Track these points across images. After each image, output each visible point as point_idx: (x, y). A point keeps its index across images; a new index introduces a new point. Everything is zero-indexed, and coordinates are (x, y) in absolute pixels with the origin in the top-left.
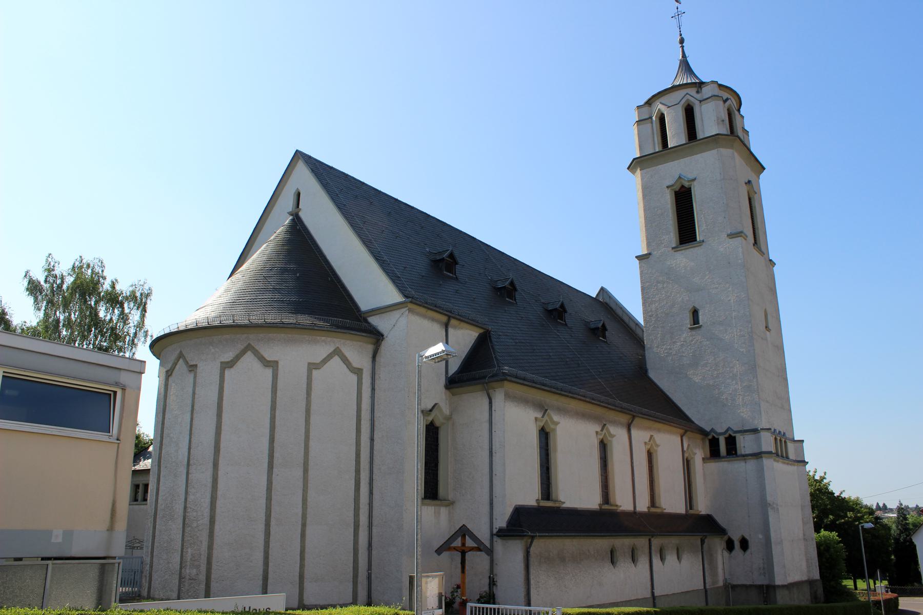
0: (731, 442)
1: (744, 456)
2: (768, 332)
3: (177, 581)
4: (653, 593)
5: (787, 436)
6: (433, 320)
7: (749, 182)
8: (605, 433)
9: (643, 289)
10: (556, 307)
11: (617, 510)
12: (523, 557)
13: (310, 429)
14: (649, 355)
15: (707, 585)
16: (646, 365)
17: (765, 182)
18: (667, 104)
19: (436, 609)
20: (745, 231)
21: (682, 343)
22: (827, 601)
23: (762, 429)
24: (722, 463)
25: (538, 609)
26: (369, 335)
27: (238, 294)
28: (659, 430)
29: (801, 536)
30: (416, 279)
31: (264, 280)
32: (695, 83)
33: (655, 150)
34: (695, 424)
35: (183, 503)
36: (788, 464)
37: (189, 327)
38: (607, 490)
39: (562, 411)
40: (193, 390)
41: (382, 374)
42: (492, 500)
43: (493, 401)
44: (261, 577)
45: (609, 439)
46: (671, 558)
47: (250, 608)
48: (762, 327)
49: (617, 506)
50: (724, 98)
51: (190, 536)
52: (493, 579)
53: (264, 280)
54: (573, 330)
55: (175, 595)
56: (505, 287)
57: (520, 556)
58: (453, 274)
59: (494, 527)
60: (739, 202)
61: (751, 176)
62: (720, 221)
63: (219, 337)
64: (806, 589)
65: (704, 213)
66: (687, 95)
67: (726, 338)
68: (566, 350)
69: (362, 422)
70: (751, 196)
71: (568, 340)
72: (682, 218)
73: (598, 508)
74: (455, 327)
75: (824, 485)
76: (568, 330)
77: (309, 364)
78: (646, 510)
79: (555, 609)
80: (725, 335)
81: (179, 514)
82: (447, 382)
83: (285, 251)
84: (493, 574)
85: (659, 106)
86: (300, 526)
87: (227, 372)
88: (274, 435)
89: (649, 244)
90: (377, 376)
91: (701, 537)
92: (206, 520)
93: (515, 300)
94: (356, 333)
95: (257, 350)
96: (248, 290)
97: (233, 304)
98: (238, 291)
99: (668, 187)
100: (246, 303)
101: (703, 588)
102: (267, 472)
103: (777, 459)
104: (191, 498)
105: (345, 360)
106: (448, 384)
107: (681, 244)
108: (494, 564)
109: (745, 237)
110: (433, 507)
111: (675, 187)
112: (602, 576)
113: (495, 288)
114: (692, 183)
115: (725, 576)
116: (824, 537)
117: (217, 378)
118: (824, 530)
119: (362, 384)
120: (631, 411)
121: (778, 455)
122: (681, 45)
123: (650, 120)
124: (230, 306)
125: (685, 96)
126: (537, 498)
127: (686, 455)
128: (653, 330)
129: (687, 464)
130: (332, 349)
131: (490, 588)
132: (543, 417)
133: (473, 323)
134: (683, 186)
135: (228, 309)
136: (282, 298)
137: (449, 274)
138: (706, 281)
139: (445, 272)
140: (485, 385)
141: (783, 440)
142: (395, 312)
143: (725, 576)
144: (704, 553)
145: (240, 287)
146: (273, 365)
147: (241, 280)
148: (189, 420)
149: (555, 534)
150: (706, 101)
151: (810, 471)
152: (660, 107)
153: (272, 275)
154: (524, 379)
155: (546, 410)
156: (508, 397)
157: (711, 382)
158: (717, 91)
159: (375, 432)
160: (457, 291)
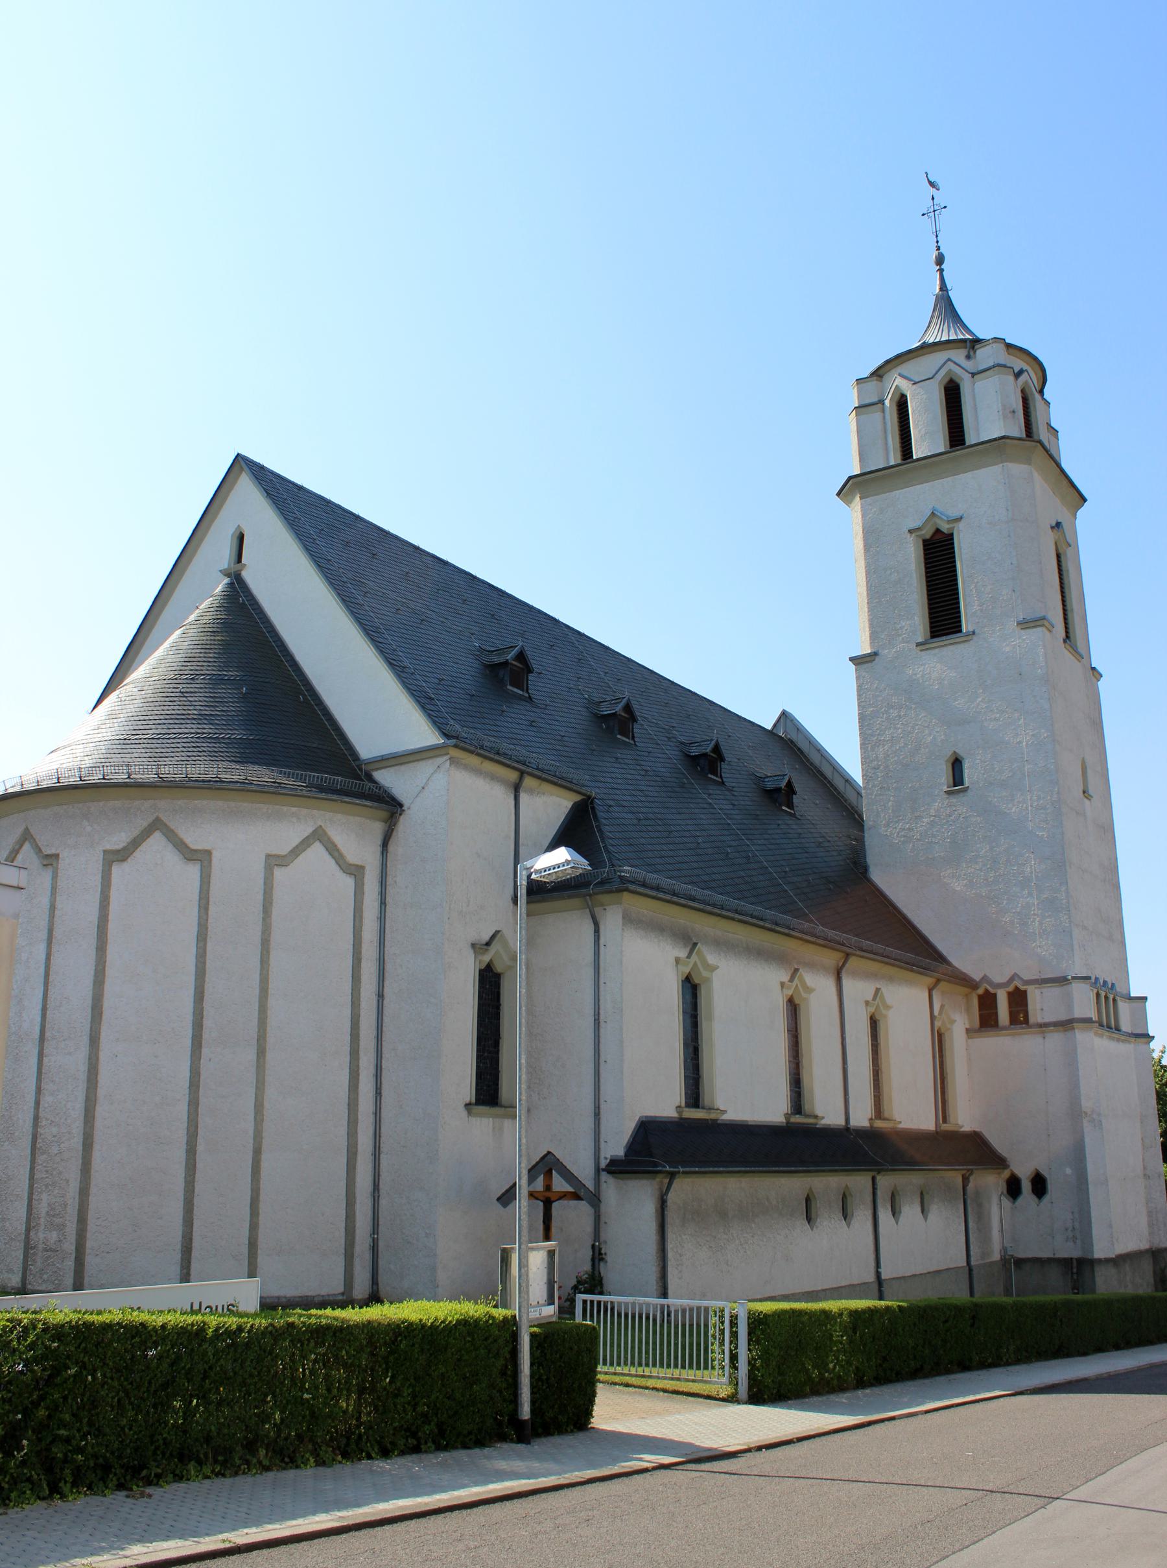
0: (1018, 999)
1: (1041, 1026)
2: (1087, 801)
3: (20, 1254)
4: (878, 1275)
5: (1118, 990)
6: (493, 777)
7: (1058, 525)
8: (797, 985)
9: (862, 718)
11: (816, 1124)
12: (654, 1210)
13: (270, 976)
14: (872, 842)
15: (972, 1259)
16: (865, 857)
17: (1085, 522)
18: (912, 378)
19: (544, 1305)
20: (1049, 616)
23: (1074, 978)
25: (686, 1302)
26: (376, 804)
27: (134, 723)
28: (891, 979)
30: (462, 701)
31: (181, 699)
32: (964, 341)
33: (888, 459)
34: (955, 967)
35: (32, 1110)
36: (1118, 1040)
37: (44, 784)
38: (800, 1088)
39: (723, 945)
40: (51, 902)
41: (399, 876)
42: (599, 1107)
43: (602, 928)
44: (179, 1247)
45: (804, 995)
46: (910, 1211)
47: (200, 1303)
49: (816, 1117)
50: (1016, 371)
51: (47, 1171)
52: (600, 1249)
53: (181, 699)
54: (735, 793)
55: (69, 1280)
57: (649, 1208)
58: (523, 691)
59: (602, 1156)
61: (1063, 516)
63: (101, 804)
64: (1147, 1266)
65: (976, 580)
67: (1013, 810)
68: (726, 832)
69: (364, 964)
70: (1061, 551)
71: (728, 812)
72: (934, 585)
74: (531, 791)
76: (727, 793)
77: (269, 856)
78: (865, 1124)
79: (735, 1305)
80: (1010, 806)
81: (24, 1130)
83: (219, 644)
84: (599, 1241)
85: (897, 382)
86: (252, 1153)
87: (116, 870)
88: (203, 986)
89: (874, 636)
90: (390, 880)
91: (964, 1172)
92: (77, 1142)
93: (633, 738)
94: (358, 801)
95: (172, 831)
96: (151, 718)
97: (125, 742)
98: (132, 719)
99: (910, 531)
100: (150, 741)
101: (965, 1264)
102: (189, 1053)
103: (1100, 1031)
104: (46, 1100)
105: (333, 850)
107: (933, 637)
111: (923, 532)
112: (791, 1244)
113: (595, 715)
114: (955, 525)
115: (1003, 1243)
117: (97, 880)
120: (843, 944)
122: (938, 267)
123: (880, 405)
124: (119, 747)
125: (945, 363)
126: (678, 1104)
127: (937, 1024)
128: (880, 795)
129: (939, 1040)
130: (310, 830)
131: (593, 1265)
132: (689, 957)
134: (938, 531)
135: (116, 751)
136: (216, 733)
137: (516, 690)
139: (509, 687)
141: (1111, 997)
143: (1003, 1243)
144: (969, 1202)
145: (138, 710)
146: (201, 858)
147: (138, 697)
148: (44, 957)
149: (711, 1169)
152: (900, 382)
153: (196, 690)
154: (657, 888)
155: (695, 944)
156: (629, 920)
158: (1003, 357)
159: (387, 983)
160: (531, 723)
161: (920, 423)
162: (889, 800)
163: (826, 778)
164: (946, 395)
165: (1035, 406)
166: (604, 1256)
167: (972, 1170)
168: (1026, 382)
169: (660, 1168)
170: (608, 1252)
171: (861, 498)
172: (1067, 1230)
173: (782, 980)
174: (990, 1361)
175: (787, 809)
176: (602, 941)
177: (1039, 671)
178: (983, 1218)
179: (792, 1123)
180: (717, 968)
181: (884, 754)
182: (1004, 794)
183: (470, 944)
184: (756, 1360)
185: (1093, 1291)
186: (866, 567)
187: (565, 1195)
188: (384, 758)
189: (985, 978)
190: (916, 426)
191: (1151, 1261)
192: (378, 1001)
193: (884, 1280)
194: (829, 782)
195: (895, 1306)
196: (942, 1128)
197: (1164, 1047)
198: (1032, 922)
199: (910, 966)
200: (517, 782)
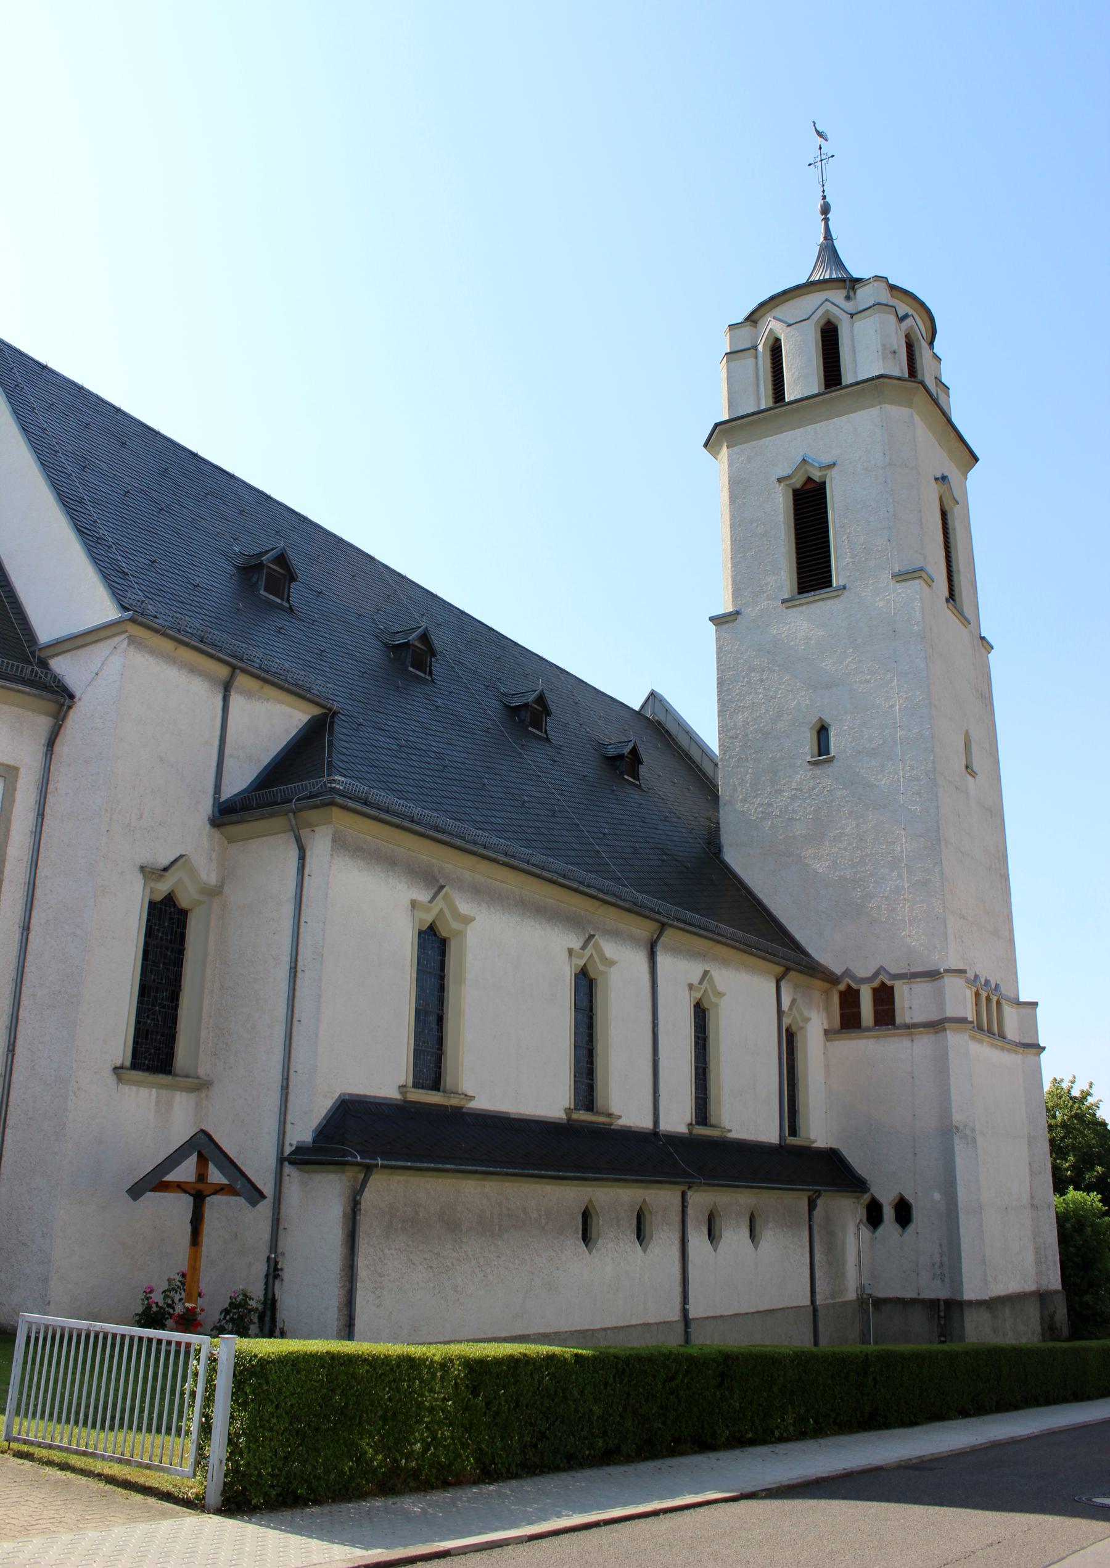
0: (884, 996)
1: (908, 1027)
4: (685, 1312)
5: (1003, 992)
6: (193, 670)
8: (592, 955)
9: (721, 683)
10: (526, 701)
11: (611, 1124)
12: (341, 1214)
14: (726, 818)
15: (818, 1297)
20: (929, 569)
21: (794, 792)
22: (1075, 1335)
23: (946, 971)
24: (865, 1041)
26: (35, 691)
28: (725, 962)
29: (1025, 1198)
36: (1003, 1049)
39: (477, 891)
43: (308, 853)
46: (735, 1236)
48: (959, 764)
49: (610, 1115)
52: (276, 1263)
56: (406, 644)
60: (920, 512)
61: (951, 470)
62: (880, 548)
64: (1033, 1312)
66: (827, 302)
67: (883, 782)
70: (947, 508)
73: (564, 1116)
74: (249, 694)
75: (1089, 1108)
78: (682, 1129)
82: (216, 810)
84: (276, 1253)
85: (771, 324)
89: (737, 593)
91: (810, 1193)
93: (431, 674)
94: (10, 685)
99: (779, 480)
101: (809, 1303)
103: (979, 1036)
106: (217, 815)
107: (800, 593)
108: (281, 1227)
109: (929, 581)
110: (154, 1090)
111: (793, 481)
113: (386, 645)
114: (828, 472)
115: (860, 1279)
116: (1074, 1203)
118: (1075, 1189)
119: (14, 801)
120: (659, 913)
121: (980, 1028)
126: (402, 1083)
127: (786, 1021)
128: (738, 767)
133: (298, 692)
137: (271, 597)
138: (847, 666)
140: (291, 814)
141: (994, 999)
142: (100, 645)
143: (860, 1279)
150: (863, 314)
151: (1062, 1080)
155: (442, 887)
156: (340, 843)
157: (848, 874)
158: (885, 296)
159: (34, 913)
161: (793, 366)
162: (747, 773)
163: (694, 762)
164: (822, 337)
165: (921, 353)
166: (280, 1273)
167: (819, 1191)
168: (911, 327)
169: (349, 1158)
170: (285, 1268)
171: (728, 447)
172: (934, 1265)
173: (571, 946)
174: (750, 1435)
175: (631, 779)
176: (307, 872)
177: (916, 627)
178: (834, 1249)
179: (574, 1120)
180: (472, 919)
181: (743, 721)
182: (874, 763)
183: (138, 866)
184: (239, 1437)
185: (962, 1338)
186: (731, 520)
187: (222, 1189)
188: (59, 640)
189: (847, 972)
190: (789, 369)
191: (1038, 1305)
192: (22, 934)
193: (693, 1319)
194: (697, 766)
195: (567, 1356)
196: (787, 1142)
197: (1074, 1077)
198: (902, 908)
199: (748, 949)
200: (228, 680)
